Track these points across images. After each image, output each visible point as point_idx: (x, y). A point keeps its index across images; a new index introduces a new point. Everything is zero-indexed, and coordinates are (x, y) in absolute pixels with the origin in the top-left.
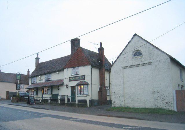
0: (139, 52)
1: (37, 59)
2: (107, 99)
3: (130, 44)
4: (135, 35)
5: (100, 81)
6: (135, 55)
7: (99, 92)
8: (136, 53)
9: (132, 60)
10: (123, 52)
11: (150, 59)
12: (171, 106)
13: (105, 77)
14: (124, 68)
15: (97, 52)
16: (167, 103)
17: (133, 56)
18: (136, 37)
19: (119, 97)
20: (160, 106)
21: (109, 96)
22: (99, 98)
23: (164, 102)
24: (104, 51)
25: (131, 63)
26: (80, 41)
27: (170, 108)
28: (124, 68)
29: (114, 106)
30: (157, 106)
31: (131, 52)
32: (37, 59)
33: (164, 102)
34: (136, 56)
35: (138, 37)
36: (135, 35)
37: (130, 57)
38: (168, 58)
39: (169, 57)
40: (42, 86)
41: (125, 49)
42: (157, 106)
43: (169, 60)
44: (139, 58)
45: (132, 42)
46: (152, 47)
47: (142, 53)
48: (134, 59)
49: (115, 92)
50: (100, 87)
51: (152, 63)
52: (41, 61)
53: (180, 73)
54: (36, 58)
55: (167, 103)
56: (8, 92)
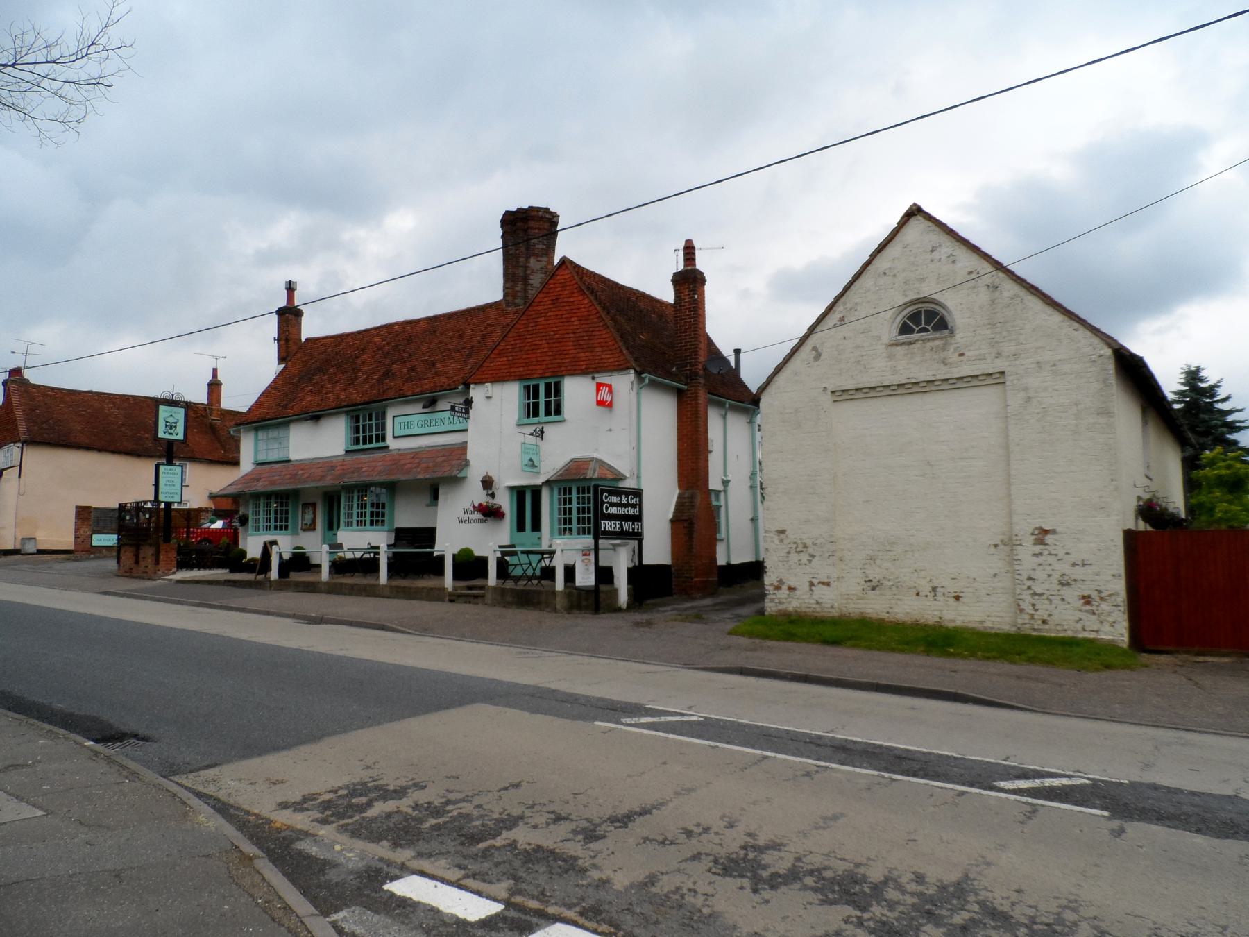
0: (931, 315)
1: (289, 316)
2: (715, 560)
3: (882, 263)
4: (915, 212)
5: (679, 460)
6: (905, 329)
7: (673, 522)
8: (915, 317)
9: (890, 357)
10: (839, 308)
11: (998, 355)
12: (1111, 619)
13: (707, 439)
14: (841, 395)
15: (666, 294)
16: (1087, 600)
17: (895, 333)
18: (917, 224)
19: (804, 558)
20: (1045, 617)
21: (395, 435)
22: (675, 554)
23: (1072, 594)
24: (706, 287)
25: (880, 370)
26: (81, 507)
27: (1107, 628)
28: (841, 395)
29: (781, 607)
30: (1032, 616)
31: (863, 314)
32: (289, 316)
33: (1072, 594)
34: (911, 331)
35: (933, 227)
36: (915, 212)
37: (879, 338)
38: (1109, 352)
39: (1110, 346)
40: (328, 482)
41: (847, 288)
42: (1032, 616)
43: (1111, 367)
44: (929, 345)
45: (893, 250)
46: (1010, 288)
47: (948, 319)
48: (900, 350)
49: (783, 532)
50: (680, 497)
51: (1009, 379)
52: (311, 327)
53: (1143, 431)
54: (281, 313)
55: (1087, 600)
56: (77, 507)
